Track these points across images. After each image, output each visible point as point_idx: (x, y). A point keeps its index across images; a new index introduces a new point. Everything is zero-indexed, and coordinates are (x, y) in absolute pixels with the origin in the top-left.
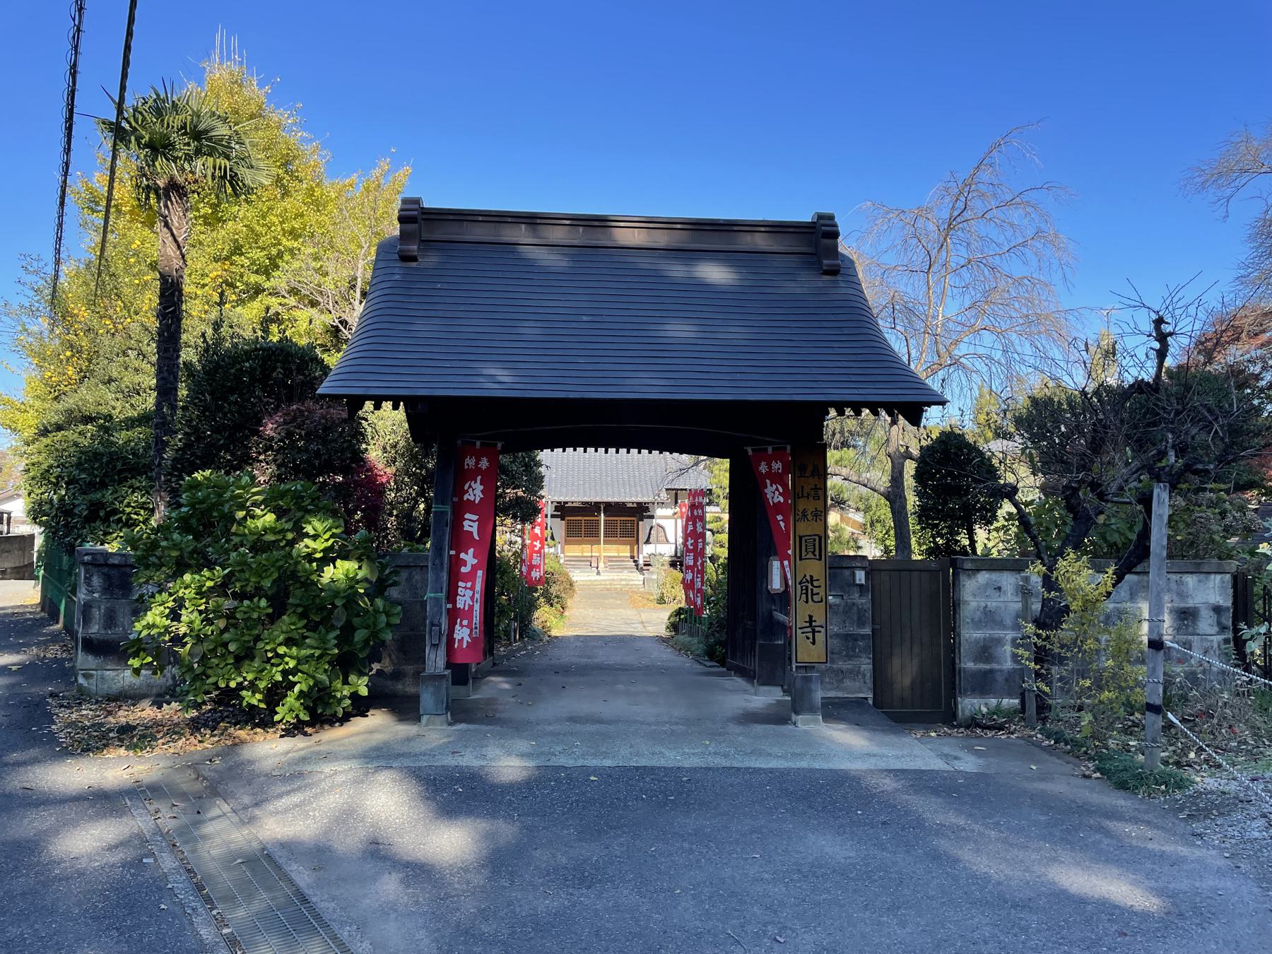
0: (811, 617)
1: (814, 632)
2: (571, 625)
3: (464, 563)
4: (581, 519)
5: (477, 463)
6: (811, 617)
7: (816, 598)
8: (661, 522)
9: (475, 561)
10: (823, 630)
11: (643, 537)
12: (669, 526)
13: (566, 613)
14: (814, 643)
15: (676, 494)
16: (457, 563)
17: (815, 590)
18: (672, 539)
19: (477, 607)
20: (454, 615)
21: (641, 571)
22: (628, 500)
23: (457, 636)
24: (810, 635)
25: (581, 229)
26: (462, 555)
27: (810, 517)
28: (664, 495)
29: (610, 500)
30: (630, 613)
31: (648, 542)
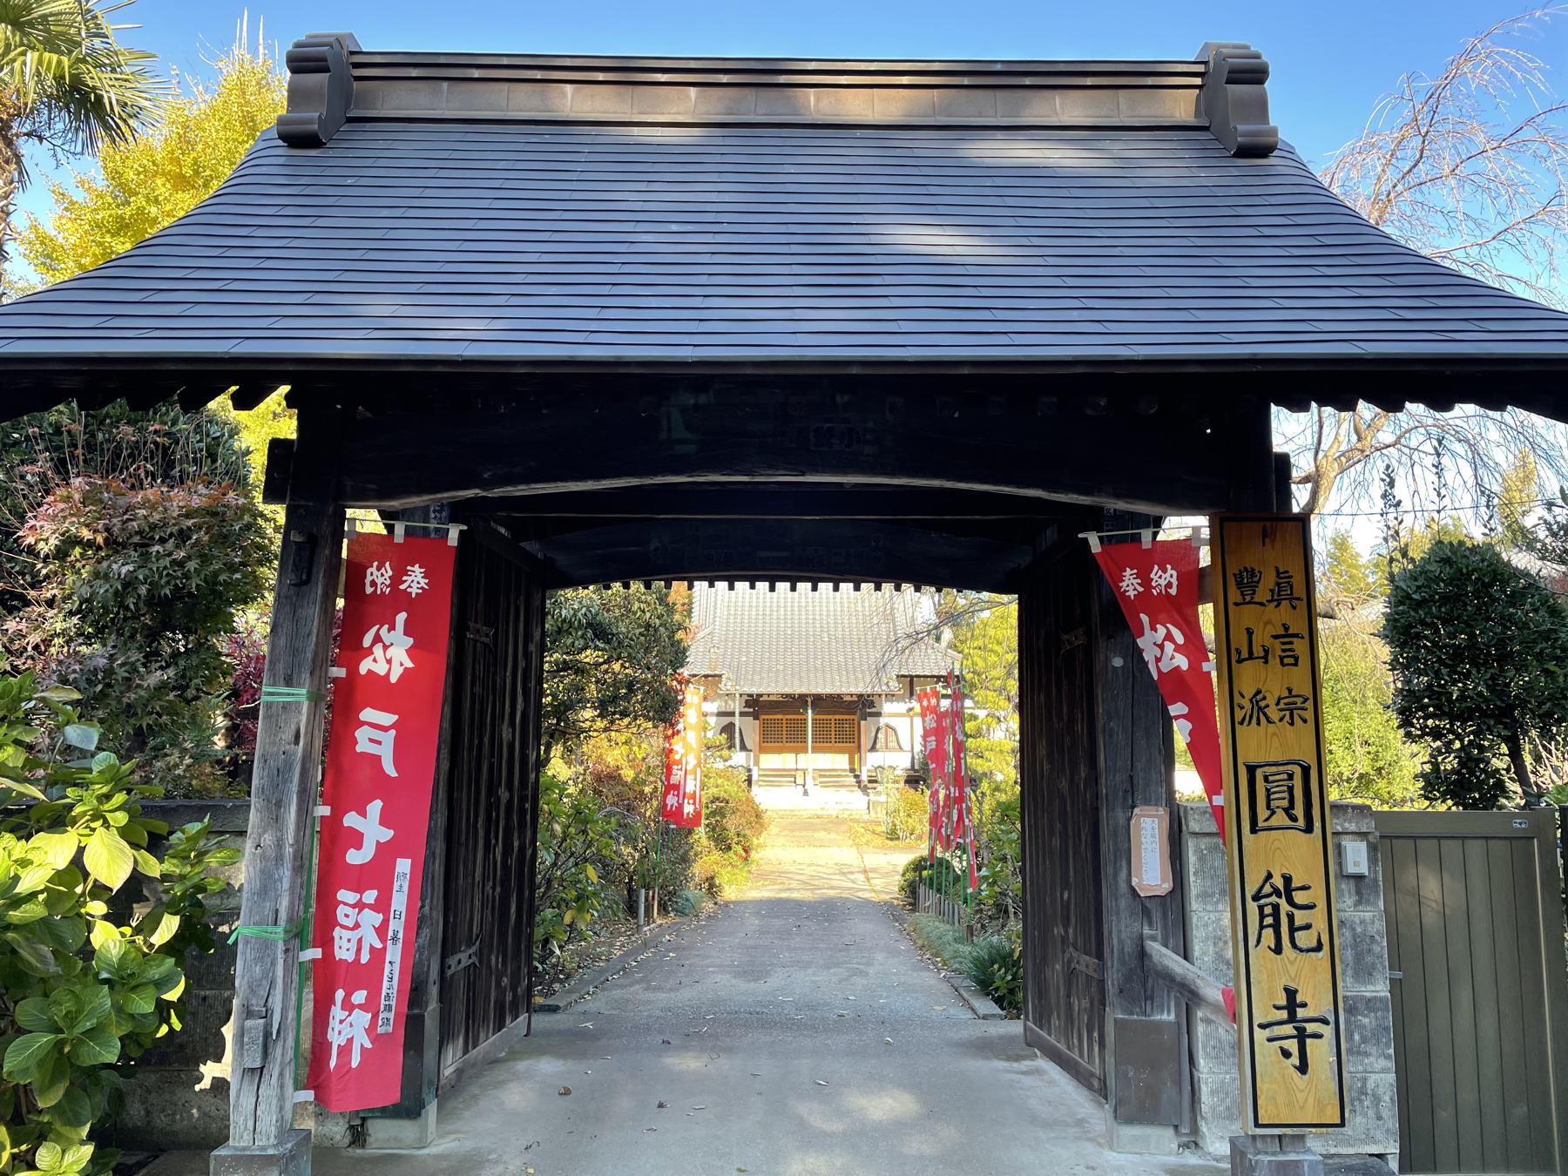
0: (1291, 994)
1: (1302, 1036)
2: (762, 876)
3: (356, 839)
4: (779, 717)
5: (396, 580)
6: (1291, 994)
7: (1301, 937)
8: (893, 722)
9: (387, 834)
10: (1327, 1031)
11: (866, 742)
12: (903, 731)
13: (753, 855)
14: (1303, 1068)
15: (910, 683)
16: (336, 838)
17: (1301, 917)
18: (906, 745)
19: (394, 954)
20: (327, 979)
21: (864, 790)
22: (844, 690)
23: (336, 1039)
24: (1292, 1045)
25: (693, 91)
26: (351, 820)
27: (1274, 713)
28: (895, 685)
29: (820, 690)
30: (847, 854)
31: (873, 748)
